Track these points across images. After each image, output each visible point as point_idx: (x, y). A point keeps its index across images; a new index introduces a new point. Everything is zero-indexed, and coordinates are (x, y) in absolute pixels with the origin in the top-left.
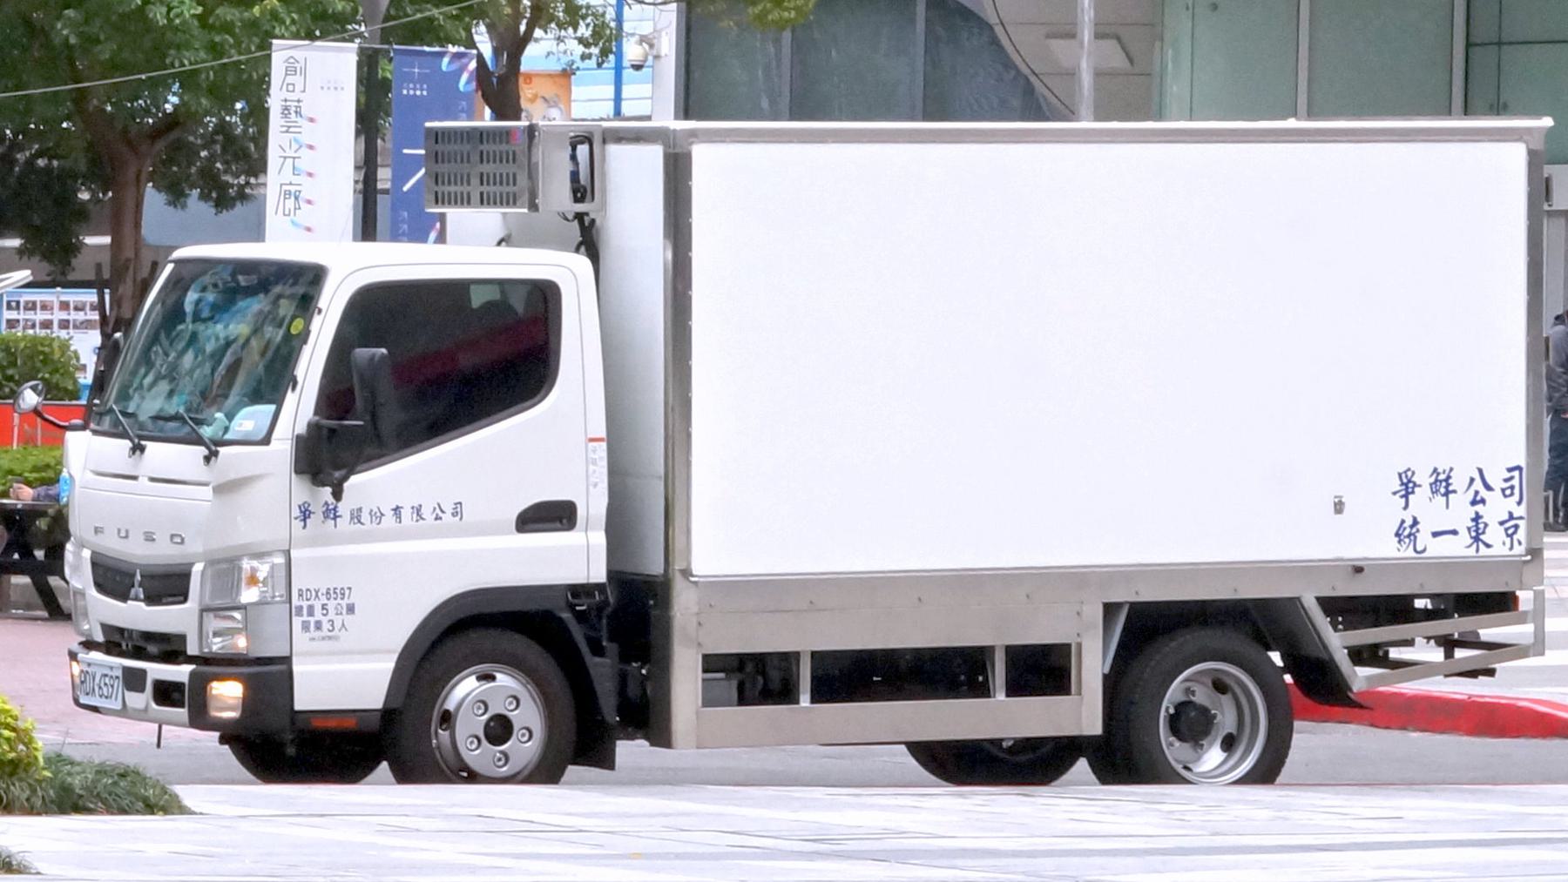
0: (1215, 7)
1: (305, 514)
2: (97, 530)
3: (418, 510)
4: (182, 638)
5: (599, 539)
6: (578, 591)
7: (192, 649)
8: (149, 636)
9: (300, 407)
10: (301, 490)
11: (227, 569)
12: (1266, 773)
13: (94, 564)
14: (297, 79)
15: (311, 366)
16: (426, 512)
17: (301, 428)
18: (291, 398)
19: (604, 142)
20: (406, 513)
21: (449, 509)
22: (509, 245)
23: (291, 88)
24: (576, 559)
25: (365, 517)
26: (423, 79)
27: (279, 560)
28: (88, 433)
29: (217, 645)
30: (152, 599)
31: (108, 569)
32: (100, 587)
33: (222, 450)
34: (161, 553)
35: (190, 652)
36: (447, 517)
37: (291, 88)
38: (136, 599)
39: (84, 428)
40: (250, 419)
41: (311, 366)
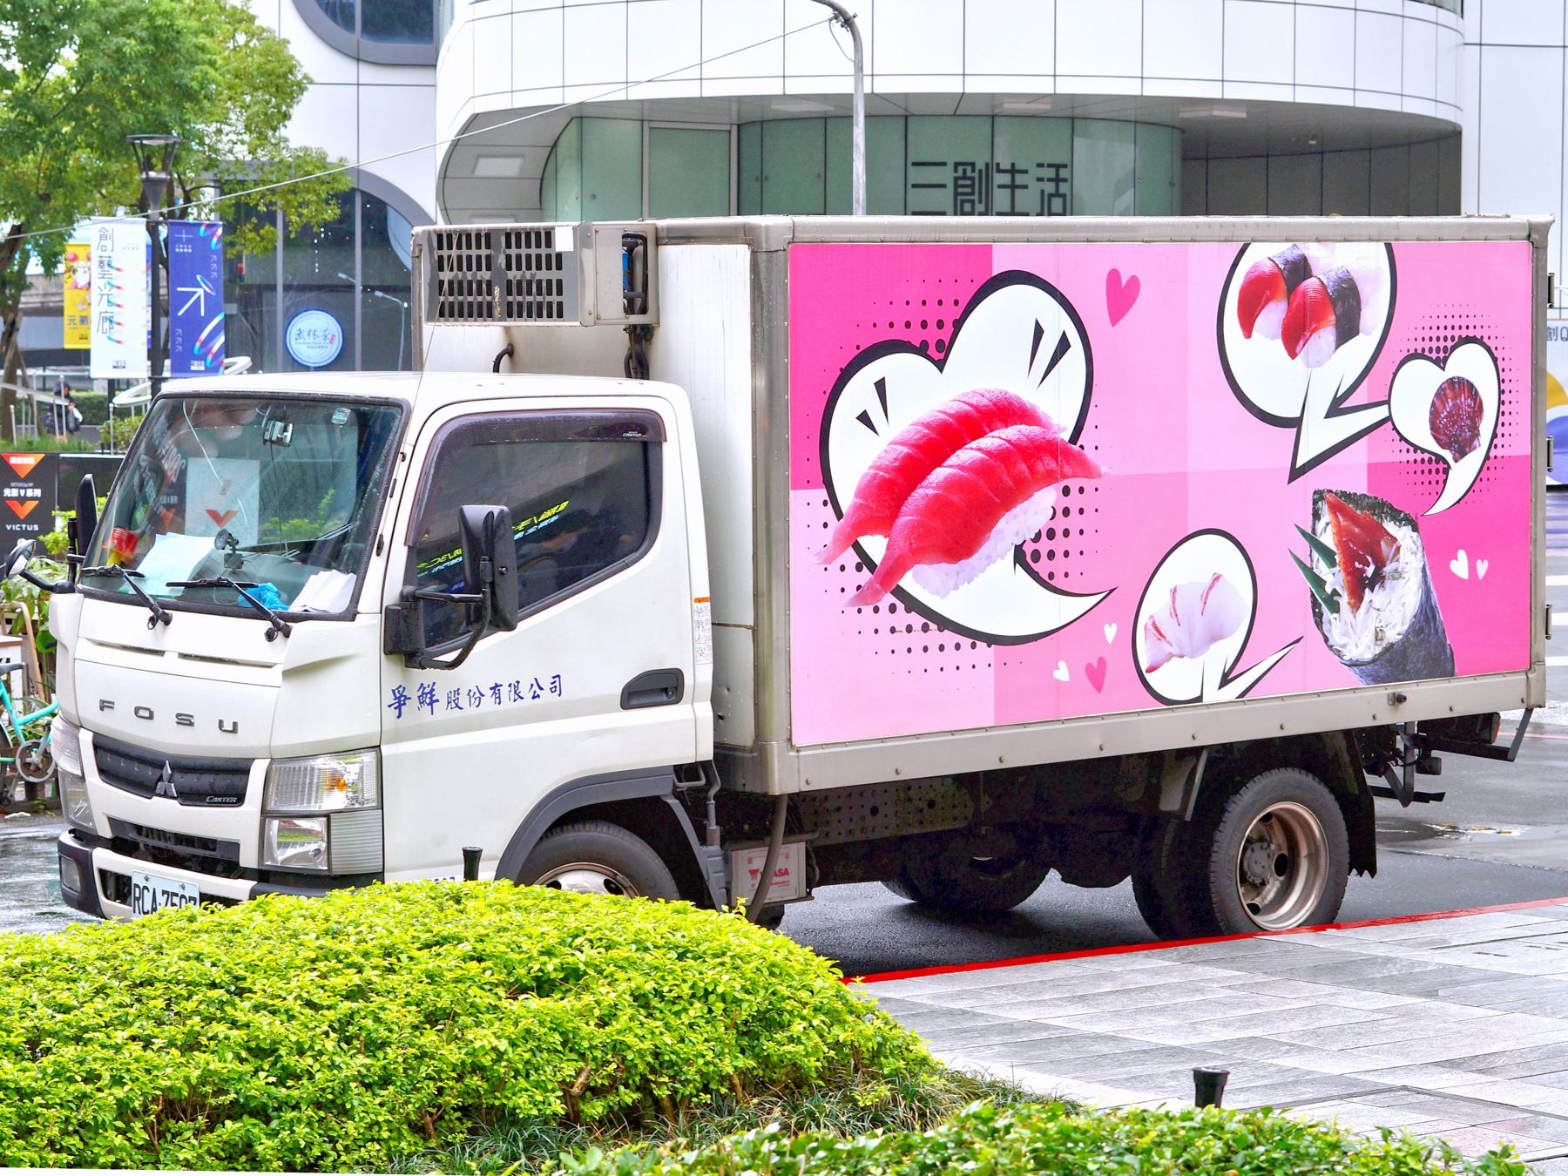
0: (594, 197)
1: (400, 701)
2: (105, 705)
3: (515, 687)
4: (235, 846)
5: (705, 711)
6: (684, 771)
7: (248, 859)
8: (181, 839)
9: (387, 575)
10: (394, 675)
11: (289, 769)
12: (1326, 918)
13: (96, 747)
14: (108, 243)
15: (396, 519)
16: (524, 689)
17: (392, 597)
18: (376, 564)
19: (657, 244)
20: (504, 690)
21: (546, 685)
22: (515, 369)
23: (104, 248)
24: (680, 735)
25: (464, 701)
26: (189, 241)
27: (369, 758)
28: (77, 596)
29: (282, 856)
30: (190, 797)
31: (102, 742)
32: (104, 772)
33: (296, 628)
34: (204, 742)
35: (243, 863)
36: (546, 695)
37: (104, 248)
38: (165, 795)
39: (70, 589)
40: (325, 588)
41: (396, 519)
